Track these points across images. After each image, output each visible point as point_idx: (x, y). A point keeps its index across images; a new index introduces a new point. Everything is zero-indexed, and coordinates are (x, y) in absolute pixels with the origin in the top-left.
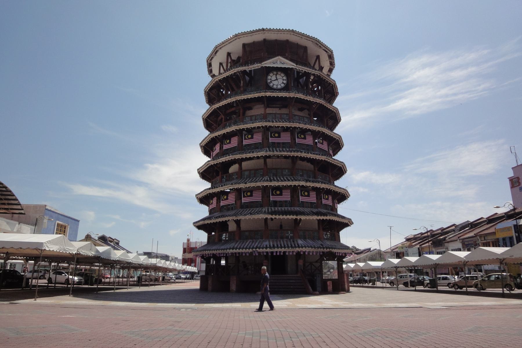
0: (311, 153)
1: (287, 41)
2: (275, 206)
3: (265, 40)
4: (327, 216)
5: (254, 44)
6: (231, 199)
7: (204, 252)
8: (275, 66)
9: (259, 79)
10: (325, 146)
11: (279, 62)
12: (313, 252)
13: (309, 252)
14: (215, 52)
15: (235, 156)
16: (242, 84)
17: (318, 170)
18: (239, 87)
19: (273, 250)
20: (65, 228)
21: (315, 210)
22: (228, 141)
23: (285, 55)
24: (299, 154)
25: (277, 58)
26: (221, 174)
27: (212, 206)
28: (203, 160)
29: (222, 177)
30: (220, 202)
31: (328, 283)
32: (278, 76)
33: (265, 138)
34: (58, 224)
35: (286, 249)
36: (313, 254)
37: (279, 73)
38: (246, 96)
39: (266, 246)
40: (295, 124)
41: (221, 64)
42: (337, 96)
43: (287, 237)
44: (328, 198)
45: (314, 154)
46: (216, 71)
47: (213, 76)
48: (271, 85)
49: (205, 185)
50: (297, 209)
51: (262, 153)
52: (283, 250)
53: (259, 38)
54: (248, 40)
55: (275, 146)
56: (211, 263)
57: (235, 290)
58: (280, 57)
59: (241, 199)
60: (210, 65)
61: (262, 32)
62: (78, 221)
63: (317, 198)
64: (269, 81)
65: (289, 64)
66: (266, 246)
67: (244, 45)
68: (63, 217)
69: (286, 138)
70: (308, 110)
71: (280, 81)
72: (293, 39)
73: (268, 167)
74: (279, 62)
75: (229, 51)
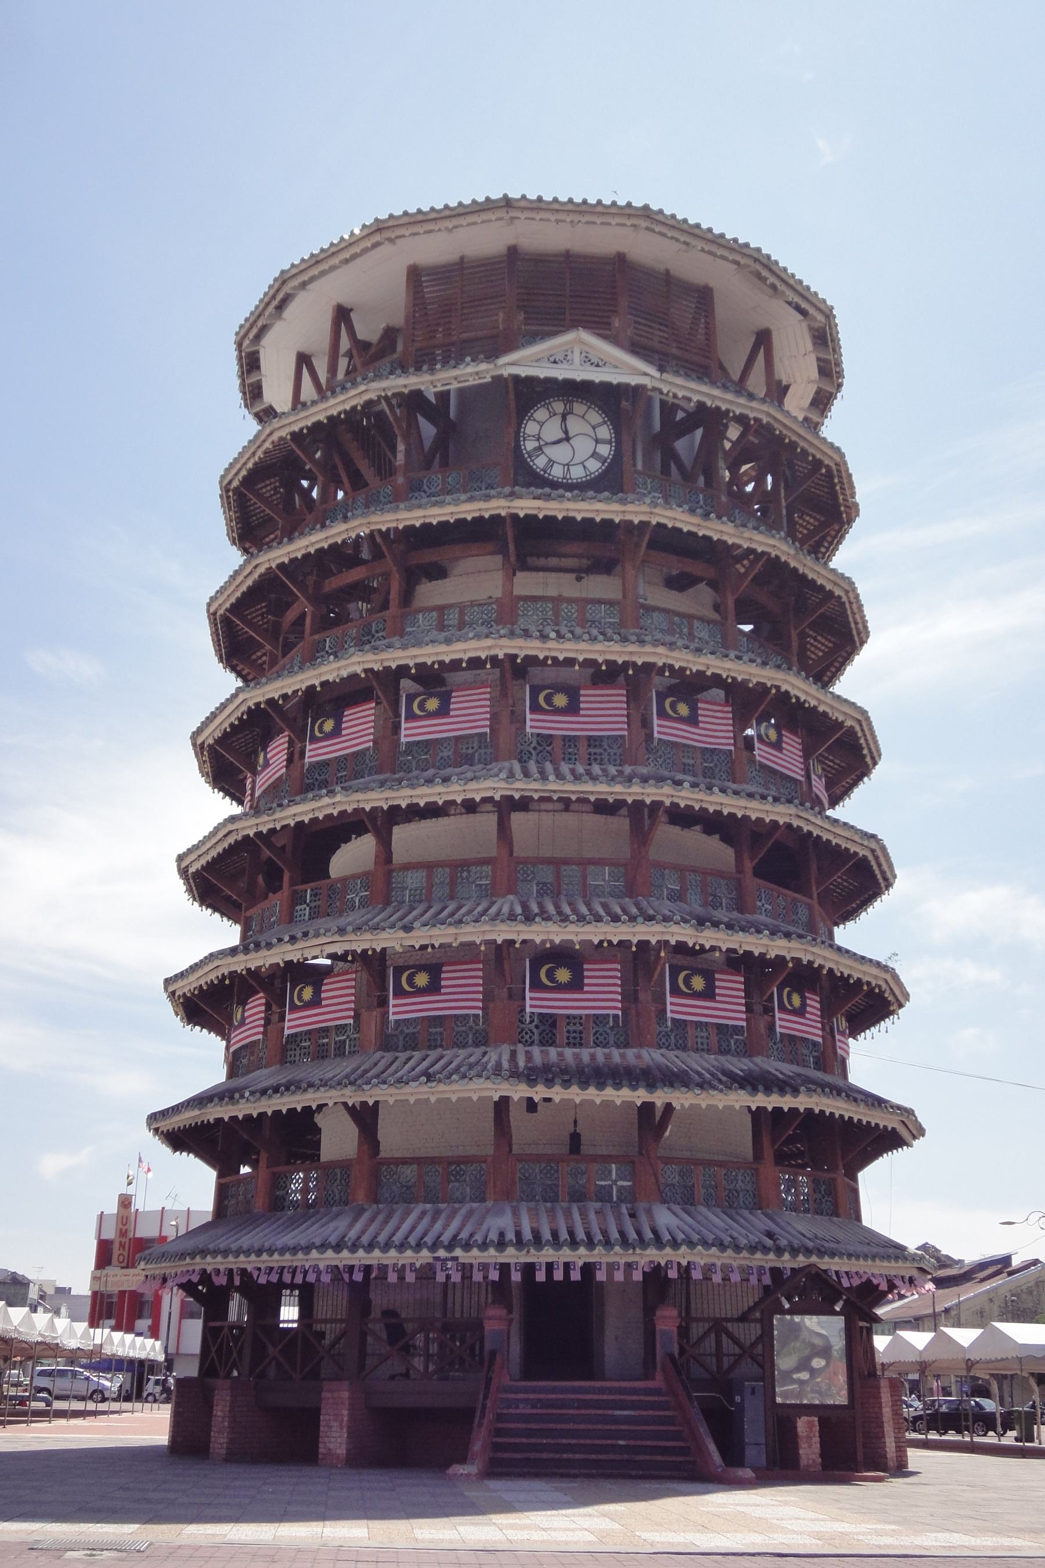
0: (723, 791)
1: (621, 259)
2: (547, 1040)
3: (513, 251)
4: (796, 1091)
5: (459, 270)
8: (560, 373)
9: (474, 435)
10: (789, 759)
11: (577, 357)
12: (727, 1269)
13: (709, 1269)
14: (279, 300)
17: (758, 873)
18: (386, 470)
22: (329, 725)
24: (664, 794)
25: (570, 336)
27: (241, 1037)
28: (207, 812)
29: (296, 899)
32: (574, 425)
36: (707, 1278)
37: (579, 408)
39: (502, 1235)
40: (648, 649)
43: (603, 1195)
44: (804, 1005)
46: (277, 393)
50: (652, 1056)
51: (489, 783)
52: (581, 1256)
53: (487, 241)
54: (435, 250)
56: (295, 1325)
58: (584, 335)
59: (383, 1003)
64: (530, 445)
66: (502, 1235)
67: (415, 274)
71: (583, 446)
72: (648, 250)
75: (346, 301)
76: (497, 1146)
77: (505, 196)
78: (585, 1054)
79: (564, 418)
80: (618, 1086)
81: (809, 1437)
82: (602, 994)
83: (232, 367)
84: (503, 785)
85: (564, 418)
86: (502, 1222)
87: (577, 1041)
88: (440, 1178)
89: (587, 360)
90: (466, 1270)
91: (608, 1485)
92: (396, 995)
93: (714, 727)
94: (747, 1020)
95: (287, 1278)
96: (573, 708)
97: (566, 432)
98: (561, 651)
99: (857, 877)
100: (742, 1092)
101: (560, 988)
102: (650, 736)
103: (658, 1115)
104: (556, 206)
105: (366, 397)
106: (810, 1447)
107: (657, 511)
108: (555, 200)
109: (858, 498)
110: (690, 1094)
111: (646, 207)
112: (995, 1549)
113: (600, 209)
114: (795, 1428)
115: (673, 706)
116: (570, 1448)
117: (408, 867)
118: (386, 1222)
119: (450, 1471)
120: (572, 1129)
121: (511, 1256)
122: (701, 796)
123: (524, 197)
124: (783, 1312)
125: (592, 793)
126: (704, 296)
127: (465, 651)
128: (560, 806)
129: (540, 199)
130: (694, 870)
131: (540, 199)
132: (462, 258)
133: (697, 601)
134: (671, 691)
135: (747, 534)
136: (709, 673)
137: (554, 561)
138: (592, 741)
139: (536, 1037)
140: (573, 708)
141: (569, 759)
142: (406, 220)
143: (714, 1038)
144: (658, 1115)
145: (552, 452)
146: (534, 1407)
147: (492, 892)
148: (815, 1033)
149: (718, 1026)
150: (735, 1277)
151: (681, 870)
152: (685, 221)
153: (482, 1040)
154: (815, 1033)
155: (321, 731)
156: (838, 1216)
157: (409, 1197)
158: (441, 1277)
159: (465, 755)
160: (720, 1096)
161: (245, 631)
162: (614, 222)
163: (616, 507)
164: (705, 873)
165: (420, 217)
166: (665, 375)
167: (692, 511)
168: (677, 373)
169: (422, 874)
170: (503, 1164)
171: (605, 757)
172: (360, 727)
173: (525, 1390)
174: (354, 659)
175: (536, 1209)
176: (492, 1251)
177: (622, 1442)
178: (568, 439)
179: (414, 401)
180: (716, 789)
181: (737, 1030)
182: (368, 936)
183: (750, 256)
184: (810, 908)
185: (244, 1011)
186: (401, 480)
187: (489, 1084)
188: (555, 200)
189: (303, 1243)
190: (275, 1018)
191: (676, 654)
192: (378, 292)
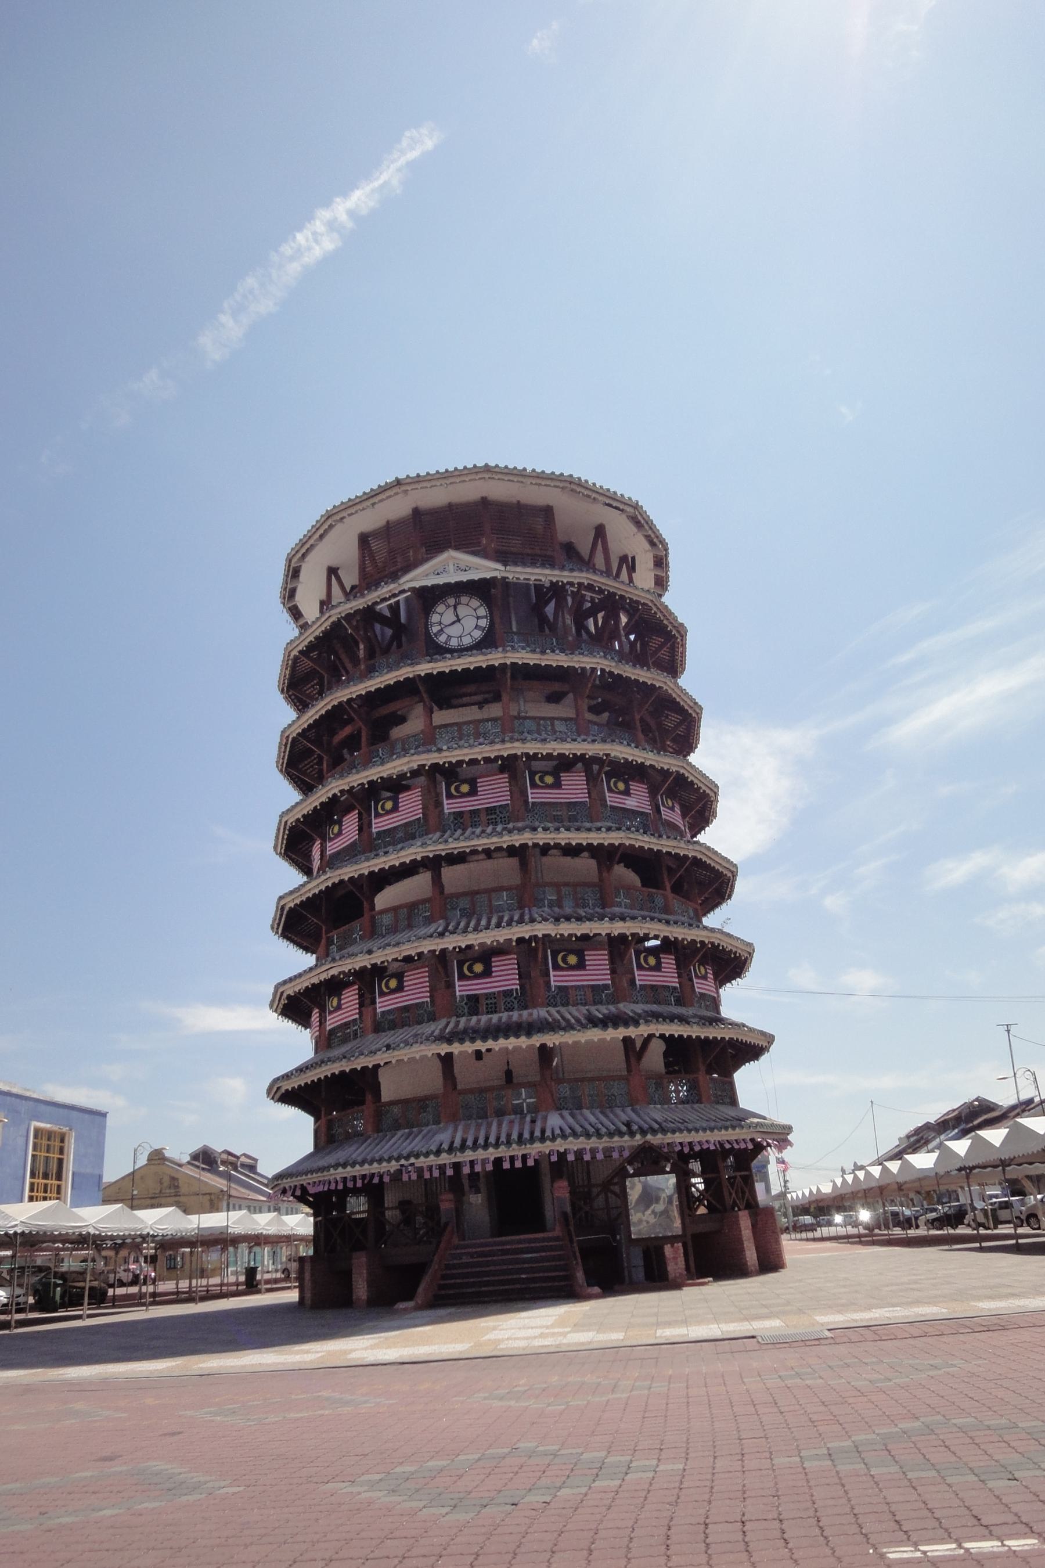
0: (568, 829)
1: (484, 502)
2: (474, 1011)
3: (416, 512)
4: (637, 1024)
5: (388, 530)
7: (303, 1180)
8: (440, 580)
9: (402, 630)
11: (451, 568)
12: (593, 1151)
13: (579, 1154)
15: (339, 872)
16: (362, 652)
18: (356, 661)
19: (459, 1158)
20: (62, 1141)
21: (600, 1011)
23: (479, 544)
24: (542, 837)
25: (444, 556)
26: (327, 932)
28: (288, 879)
29: (330, 942)
30: (374, 1002)
31: (668, 1249)
32: (462, 611)
33: (433, 803)
34: (38, 1132)
35: (503, 1152)
36: (593, 1157)
37: (464, 599)
38: (362, 686)
40: (508, 745)
41: (332, 572)
42: (683, 637)
43: (518, 1110)
44: (706, 973)
45: (578, 829)
46: (310, 611)
47: (304, 627)
48: (442, 639)
49: (296, 962)
50: (540, 1013)
51: (412, 850)
52: (492, 1153)
53: (398, 508)
54: (370, 520)
55: (463, 821)
56: (364, 1215)
57: (364, 1297)
58: (452, 553)
60: (293, 573)
61: (395, 490)
62: (104, 1115)
63: (613, 971)
64: (435, 629)
67: (364, 540)
68: (49, 1108)
69: (495, 791)
71: (469, 623)
72: (499, 491)
73: (447, 891)
75: (334, 564)
76: (445, 1086)
77: (397, 478)
78: (495, 1018)
80: (507, 1037)
81: (675, 1258)
82: (505, 976)
83: (287, 616)
84: (420, 850)
86: (444, 1137)
87: (493, 1010)
88: (415, 1112)
89: (459, 568)
90: (420, 1171)
91: (468, 1309)
92: (459, 979)
93: (495, 791)
94: (680, 983)
95: (350, 1185)
97: (457, 616)
98: (453, 756)
100: (595, 1030)
101: (478, 976)
102: (526, 802)
103: (638, 1045)
104: (429, 477)
105: (331, 620)
106: (676, 1264)
107: (545, 657)
108: (428, 474)
109: (680, 620)
110: (556, 1036)
111: (486, 465)
112: (868, 1320)
113: (457, 473)
114: (663, 1253)
115: (615, 784)
116: (488, 1284)
117: (382, 912)
119: (396, 1306)
120: (506, 1068)
121: (445, 1159)
122: (552, 835)
123: (408, 476)
125: (479, 845)
126: (548, 512)
127: (395, 767)
128: (482, 856)
129: (418, 475)
130: (566, 884)
131: (418, 475)
132: (388, 522)
133: (564, 710)
135: (576, 659)
136: (555, 754)
137: (465, 700)
138: (490, 811)
141: (474, 825)
142: (343, 507)
143: (589, 994)
144: (638, 1045)
145: (449, 631)
146: (472, 1257)
147: (429, 920)
148: (673, 981)
149: (592, 986)
150: (600, 1156)
151: (557, 886)
152: (515, 468)
153: (433, 1018)
154: (673, 981)
155: (383, 808)
156: (700, 1101)
157: (397, 1126)
158: (405, 1178)
159: (408, 833)
160: (580, 1034)
161: (302, 760)
162: (506, 478)
163: (481, 658)
164: (575, 885)
165: (351, 503)
166: (508, 568)
167: (533, 651)
168: (516, 564)
169: (390, 915)
170: (453, 1099)
171: (499, 820)
172: (411, 806)
173: (496, 1244)
174: (332, 785)
175: (469, 1125)
176: (432, 1157)
177: (524, 1276)
178: (459, 620)
180: (562, 829)
181: (606, 987)
182: (349, 961)
183: (565, 481)
184: (665, 897)
185: (340, 1000)
186: (363, 667)
187: (423, 1047)
188: (428, 474)
189: (341, 1161)
191: (528, 745)
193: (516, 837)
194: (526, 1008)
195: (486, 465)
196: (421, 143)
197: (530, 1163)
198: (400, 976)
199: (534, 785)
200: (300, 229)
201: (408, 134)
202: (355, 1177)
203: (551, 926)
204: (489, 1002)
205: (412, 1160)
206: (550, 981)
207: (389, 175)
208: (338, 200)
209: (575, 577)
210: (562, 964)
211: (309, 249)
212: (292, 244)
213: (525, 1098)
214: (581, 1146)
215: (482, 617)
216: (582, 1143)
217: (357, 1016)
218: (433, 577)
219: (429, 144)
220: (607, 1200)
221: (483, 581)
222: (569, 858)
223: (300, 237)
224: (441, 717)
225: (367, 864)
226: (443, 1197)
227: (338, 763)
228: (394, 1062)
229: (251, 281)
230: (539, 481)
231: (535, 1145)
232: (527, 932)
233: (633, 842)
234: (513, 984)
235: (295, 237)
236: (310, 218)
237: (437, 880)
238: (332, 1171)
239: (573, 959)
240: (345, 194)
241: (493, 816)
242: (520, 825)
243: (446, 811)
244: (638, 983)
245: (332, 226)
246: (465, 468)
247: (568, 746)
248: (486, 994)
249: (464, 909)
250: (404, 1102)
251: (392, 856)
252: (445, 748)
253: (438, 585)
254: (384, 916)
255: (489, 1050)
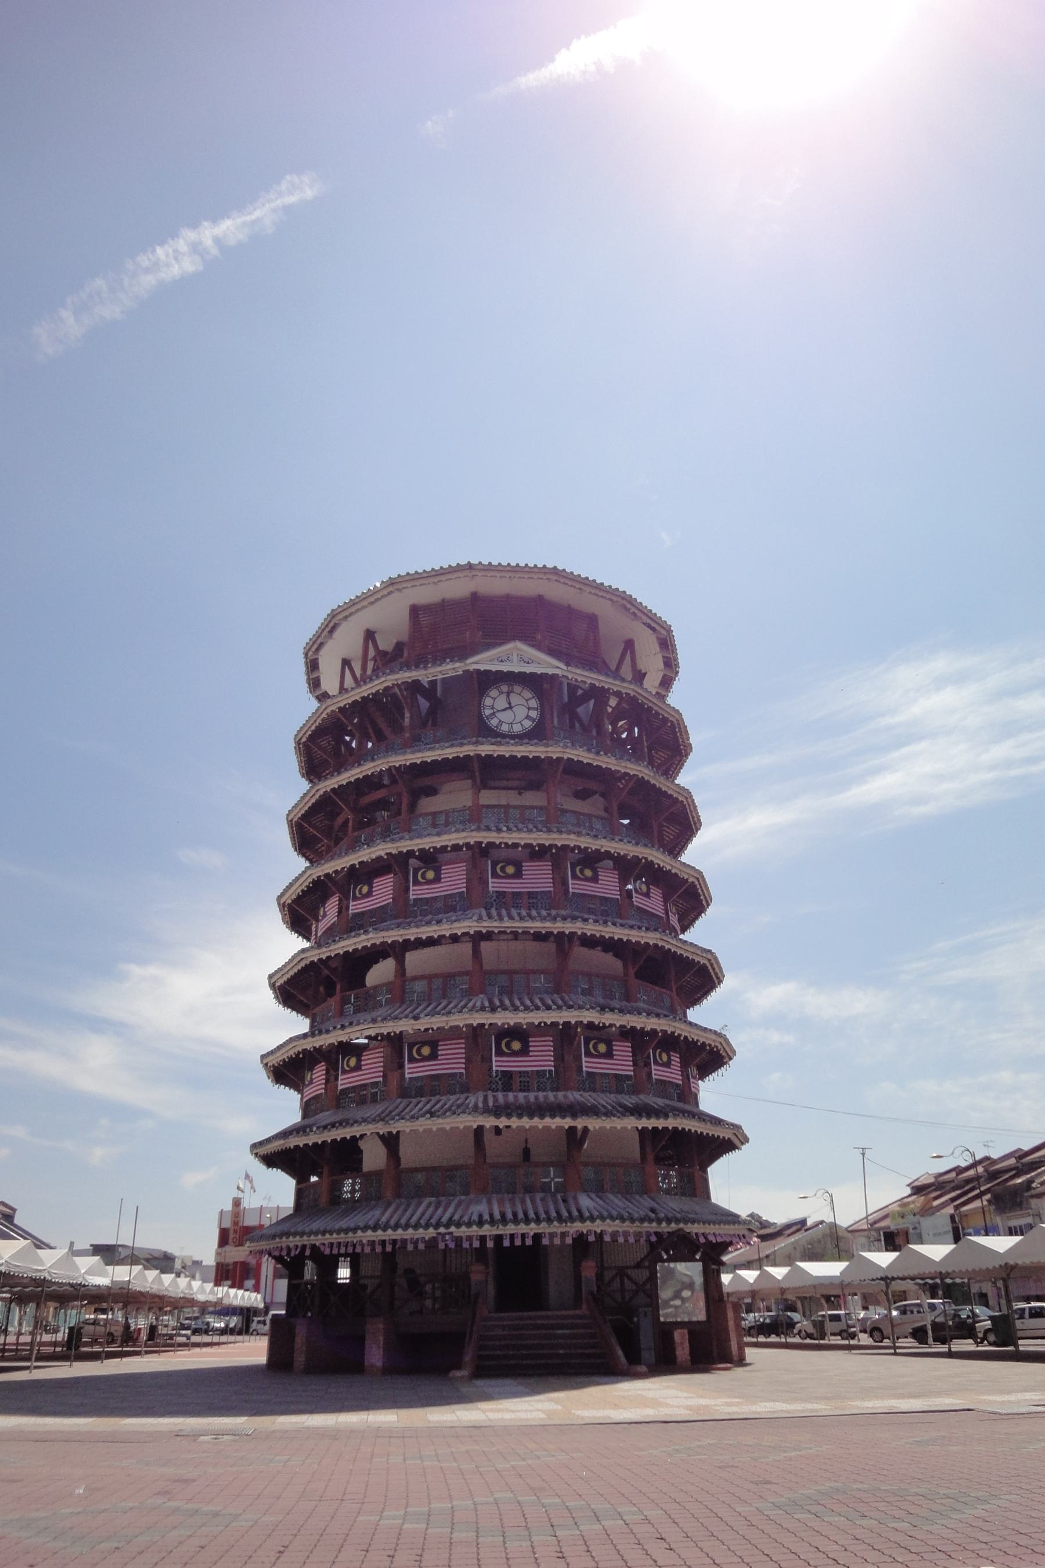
0: (614, 924)
1: (540, 598)
2: (507, 1088)
3: (474, 596)
4: (666, 1116)
5: (443, 607)
6: (372, 1069)
8: (505, 668)
9: (453, 707)
10: (655, 903)
11: (515, 658)
13: (615, 1235)
14: (330, 627)
19: (500, 1230)
21: (629, 1100)
24: (578, 927)
27: (310, 1092)
28: (287, 947)
29: (345, 1001)
32: (515, 699)
33: (476, 879)
35: (543, 1228)
37: (517, 688)
39: (481, 1216)
40: (564, 836)
41: (346, 663)
43: (545, 1188)
46: (330, 683)
47: (322, 697)
49: (291, 1026)
50: (575, 1096)
51: (466, 923)
52: (532, 1229)
53: (458, 589)
55: (504, 902)
57: (379, 1364)
58: (519, 644)
60: (313, 666)
64: (488, 712)
65: (545, 664)
66: (481, 1216)
67: (415, 611)
69: (538, 878)
70: (603, 795)
71: (521, 712)
72: (555, 592)
74: (515, 658)
78: (521, 1096)
79: (508, 696)
80: (553, 1116)
81: (682, 1343)
82: (542, 1057)
85: (508, 696)
86: (480, 1208)
87: (525, 1088)
89: (522, 660)
90: (458, 1240)
93: (608, 885)
94: (634, 1071)
96: (518, 874)
97: (510, 704)
99: (700, 977)
100: (632, 1118)
101: (515, 1054)
105: (385, 685)
110: (599, 1120)
113: (527, 569)
117: (415, 978)
118: (406, 1210)
121: (487, 1230)
122: (600, 928)
123: (480, 563)
124: (664, 1261)
127: (450, 840)
132: (443, 600)
134: (579, 862)
139: (500, 1087)
140: (518, 874)
145: (501, 716)
147: (470, 993)
148: (677, 1078)
151: (589, 976)
153: (466, 1089)
154: (677, 1078)
157: (419, 1193)
158: (442, 1246)
159: (451, 906)
161: (311, 831)
170: (479, 1170)
172: (384, 890)
174: (380, 847)
176: (475, 1228)
179: (415, 686)
180: (609, 923)
181: (628, 1077)
182: (391, 1024)
190: (332, 1078)
191: (582, 839)
192: (392, 622)
193: (569, 925)
194: (557, 1090)
195: (555, 568)
196: (299, 190)
197: (569, 1241)
198: (434, 1045)
199: (495, 875)
200: (162, 243)
201: (288, 177)
202: (340, 1243)
203: (597, 1015)
204: (522, 1079)
205: (453, 1229)
206: (581, 1066)
207: (263, 212)
208: (206, 224)
209: (624, 687)
210: (593, 1051)
211: (168, 265)
212: (151, 257)
213: (553, 1178)
214: (616, 1229)
215: (533, 709)
216: (617, 1226)
217: (381, 1079)
218: (496, 662)
219: (309, 193)
220: (622, 1283)
221: (543, 677)
222: (586, 950)
223: (160, 251)
224: (488, 797)
225: (415, 930)
226: (473, 1268)
227: (341, 760)
228: (368, 1134)
229: (100, 283)
230: (597, 592)
231: (575, 1224)
232: (573, 1017)
233: (664, 944)
234: (547, 1064)
235: (154, 251)
236: (175, 235)
237: (476, 953)
238: (359, 1233)
239: (602, 1048)
240: (215, 220)
241: (531, 901)
242: (563, 912)
243: (490, 889)
244: (654, 1077)
245: (196, 248)
246: (535, 566)
247: (614, 845)
248: (520, 1072)
249: (503, 987)
250: (428, 1170)
251: (445, 926)
252: (584, 832)
253: (502, 672)
254: (417, 983)
255: (508, 1127)
